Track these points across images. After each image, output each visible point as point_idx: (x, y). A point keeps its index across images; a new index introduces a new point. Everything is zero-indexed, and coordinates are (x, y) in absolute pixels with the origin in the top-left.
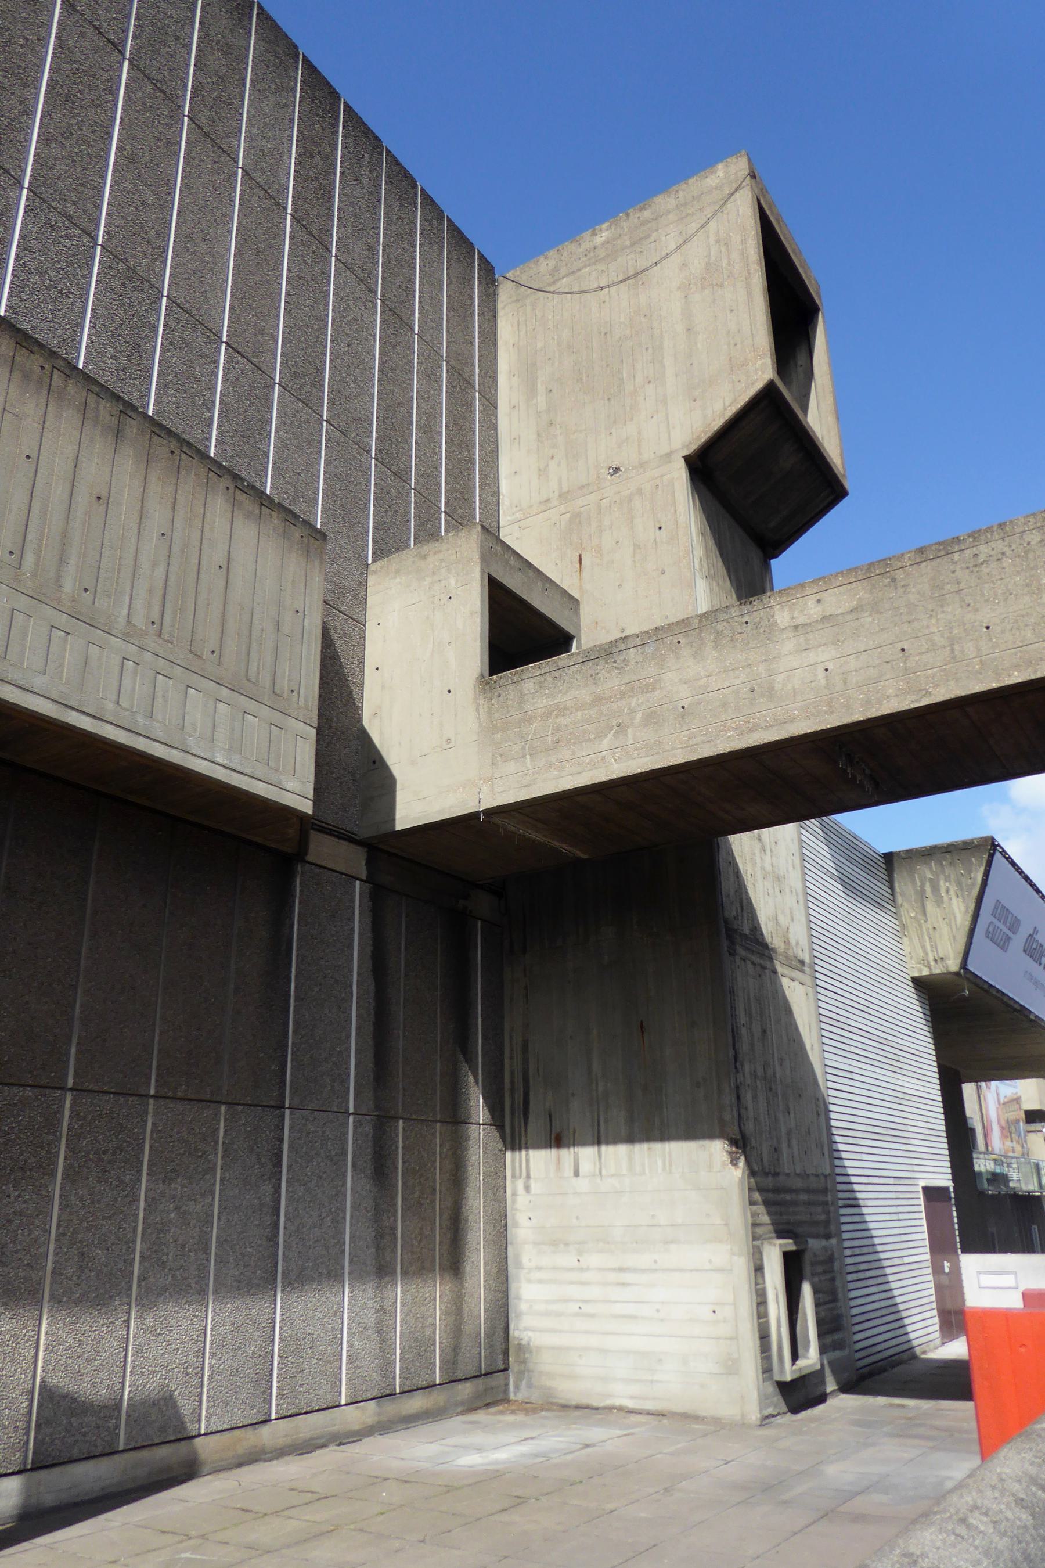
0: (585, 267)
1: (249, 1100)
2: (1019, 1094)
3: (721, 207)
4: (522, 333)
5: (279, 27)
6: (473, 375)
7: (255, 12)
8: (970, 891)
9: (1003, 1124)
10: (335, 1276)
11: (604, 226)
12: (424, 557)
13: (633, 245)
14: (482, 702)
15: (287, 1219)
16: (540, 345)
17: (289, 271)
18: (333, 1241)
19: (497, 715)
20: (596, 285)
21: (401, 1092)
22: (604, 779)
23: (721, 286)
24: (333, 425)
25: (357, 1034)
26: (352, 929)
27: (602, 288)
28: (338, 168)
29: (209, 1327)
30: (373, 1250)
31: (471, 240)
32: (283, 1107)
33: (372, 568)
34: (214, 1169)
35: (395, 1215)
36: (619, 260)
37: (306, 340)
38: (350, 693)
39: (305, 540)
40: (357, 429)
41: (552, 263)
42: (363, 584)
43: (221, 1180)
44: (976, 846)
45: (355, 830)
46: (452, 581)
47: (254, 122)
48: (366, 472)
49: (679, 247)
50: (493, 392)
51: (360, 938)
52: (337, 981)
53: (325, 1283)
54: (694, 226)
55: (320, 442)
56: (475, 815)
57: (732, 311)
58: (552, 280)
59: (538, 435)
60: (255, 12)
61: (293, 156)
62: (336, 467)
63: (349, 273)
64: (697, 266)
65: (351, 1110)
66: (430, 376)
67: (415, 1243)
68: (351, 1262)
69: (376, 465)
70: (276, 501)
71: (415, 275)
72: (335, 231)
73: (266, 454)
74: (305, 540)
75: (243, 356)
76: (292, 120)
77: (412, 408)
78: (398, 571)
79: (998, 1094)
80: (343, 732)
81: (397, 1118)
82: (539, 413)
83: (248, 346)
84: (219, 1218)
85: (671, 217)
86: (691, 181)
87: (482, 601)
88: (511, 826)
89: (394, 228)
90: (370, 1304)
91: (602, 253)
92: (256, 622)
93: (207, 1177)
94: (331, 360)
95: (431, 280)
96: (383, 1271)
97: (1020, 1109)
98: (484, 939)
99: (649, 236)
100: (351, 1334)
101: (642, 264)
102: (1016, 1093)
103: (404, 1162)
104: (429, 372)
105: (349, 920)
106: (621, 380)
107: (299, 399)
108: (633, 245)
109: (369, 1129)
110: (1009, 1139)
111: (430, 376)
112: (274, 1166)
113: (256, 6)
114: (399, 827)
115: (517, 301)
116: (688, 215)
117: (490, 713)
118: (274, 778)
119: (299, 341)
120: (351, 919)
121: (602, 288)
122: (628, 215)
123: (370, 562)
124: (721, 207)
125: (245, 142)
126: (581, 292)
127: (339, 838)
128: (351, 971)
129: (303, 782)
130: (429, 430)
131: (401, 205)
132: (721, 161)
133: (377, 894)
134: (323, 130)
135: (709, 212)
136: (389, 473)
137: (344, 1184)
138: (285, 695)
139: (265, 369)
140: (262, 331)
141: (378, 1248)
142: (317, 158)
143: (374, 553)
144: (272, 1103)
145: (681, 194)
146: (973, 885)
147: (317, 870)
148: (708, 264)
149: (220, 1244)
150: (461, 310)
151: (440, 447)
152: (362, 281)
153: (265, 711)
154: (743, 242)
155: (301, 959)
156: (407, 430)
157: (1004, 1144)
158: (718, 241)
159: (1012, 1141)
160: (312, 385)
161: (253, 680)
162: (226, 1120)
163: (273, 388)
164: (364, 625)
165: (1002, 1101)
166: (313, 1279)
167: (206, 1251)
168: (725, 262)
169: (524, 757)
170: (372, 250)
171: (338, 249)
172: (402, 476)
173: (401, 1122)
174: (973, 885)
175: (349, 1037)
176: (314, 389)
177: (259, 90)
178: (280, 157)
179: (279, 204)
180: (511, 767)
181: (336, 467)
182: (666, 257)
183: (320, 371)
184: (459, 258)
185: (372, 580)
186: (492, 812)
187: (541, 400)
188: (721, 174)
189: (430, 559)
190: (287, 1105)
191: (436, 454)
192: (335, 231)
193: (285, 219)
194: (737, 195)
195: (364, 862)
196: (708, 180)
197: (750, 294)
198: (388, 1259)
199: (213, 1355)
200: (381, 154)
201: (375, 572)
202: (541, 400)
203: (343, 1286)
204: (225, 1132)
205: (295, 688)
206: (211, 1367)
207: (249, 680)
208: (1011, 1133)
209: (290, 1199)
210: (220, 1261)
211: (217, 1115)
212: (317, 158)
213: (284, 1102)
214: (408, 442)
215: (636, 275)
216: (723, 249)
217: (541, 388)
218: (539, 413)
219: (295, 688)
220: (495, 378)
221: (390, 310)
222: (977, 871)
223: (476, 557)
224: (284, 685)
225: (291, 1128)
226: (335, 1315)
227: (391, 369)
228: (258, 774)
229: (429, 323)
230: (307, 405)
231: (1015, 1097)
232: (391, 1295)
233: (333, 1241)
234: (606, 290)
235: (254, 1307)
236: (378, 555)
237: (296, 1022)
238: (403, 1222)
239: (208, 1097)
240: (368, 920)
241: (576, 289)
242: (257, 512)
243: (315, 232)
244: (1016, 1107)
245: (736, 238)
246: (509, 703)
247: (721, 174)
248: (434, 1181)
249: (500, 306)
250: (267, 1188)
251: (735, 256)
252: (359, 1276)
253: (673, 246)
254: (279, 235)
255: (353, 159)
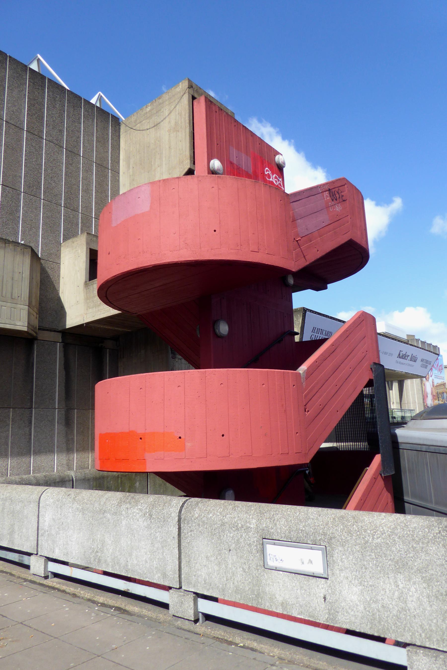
0: (144, 120)
1: (20, 407)
2: (445, 382)
3: (180, 100)
4: (127, 145)
5: (19, 62)
6: (108, 164)
7: (8, 60)
8: (298, 326)
9: (434, 394)
10: (52, 451)
11: (149, 104)
12: (73, 242)
13: (157, 112)
14: (85, 290)
15: (34, 437)
16: (131, 149)
17: (26, 151)
18: (50, 442)
19: (88, 294)
20: (146, 128)
21: (76, 402)
22: (110, 315)
23: (178, 131)
24: (45, 200)
25: (58, 387)
26: (56, 357)
27: (148, 129)
28: (46, 105)
29: (9, 463)
30: (65, 444)
31: (108, 111)
32: (32, 408)
33: (62, 245)
34: (9, 425)
35: (74, 435)
36: (153, 118)
37: (33, 174)
38: (54, 286)
39: (23, 250)
40: (55, 198)
41: (135, 117)
42: (59, 251)
43: (12, 428)
44: (299, 311)
45: (57, 328)
46: (80, 251)
47: (9, 102)
48: (60, 212)
49: (169, 115)
50: (118, 167)
51: (59, 359)
52: (50, 372)
53: (48, 453)
54: (173, 107)
55: (40, 207)
56: (83, 325)
57: (181, 141)
58: (135, 125)
59: (130, 184)
60: (8, 60)
61: (26, 108)
62: (47, 214)
63: (51, 143)
64: (173, 122)
65: (57, 408)
66: (88, 170)
67: (81, 442)
68: (57, 447)
69: (64, 209)
70: (11, 240)
71: (81, 134)
72: (45, 130)
73: (19, 217)
74: (23, 250)
75: (8, 187)
76: (25, 95)
77: (80, 184)
78: (68, 247)
79: (433, 382)
80: (52, 299)
81: (75, 409)
82: (130, 175)
83: (10, 183)
84: (11, 437)
85: (167, 103)
86: (173, 89)
87: (86, 258)
88: (97, 326)
89: (71, 119)
90: (64, 458)
91: (148, 115)
92: (4, 279)
93: (7, 427)
94: (44, 177)
95: (88, 134)
96: (69, 450)
97: (445, 388)
98: (110, 355)
99: (160, 110)
100: (57, 466)
101: (159, 120)
102: (444, 382)
103: (77, 421)
104: (87, 169)
105: (55, 355)
106: (152, 165)
107: (31, 195)
108: (157, 112)
109: (63, 412)
110: (437, 400)
111: (88, 170)
112: (29, 423)
113: (8, 57)
114: (67, 327)
115: (126, 132)
116: (171, 102)
117: (86, 294)
118: (13, 323)
119: (31, 175)
120: (56, 354)
121: (148, 129)
122: (155, 100)
123: (62, 243)
124: (180, 100)
125: (6, 111)
126: (143, 130)
127: (51, 331)
128: (56, 369)
129: (23, 322)
130: (87, 191)
131: (74, 109)
132: (181, 82)
133: (66, 346)
134: (39, 93)
135: (177, 101)
136: (69, 210)
137: (55, 427)
138: (16, 299)
139: (17, 189)
140: (16, 176)
141: (67, 444)
142: (36, 105)
143: (63, 239)
144: (28, 407)
145: (170, 94)
146: (299, 324)
147: (42, 342)
148: (176, 122)
149: (12, 443)
150: (102, 141)
151: (92, 195)
152: (57, 145)
153: (9, 304)
154: (185, 115)
155: (37, 367)
156: (78, 193)
157: (433, 402)
158: (178, 114)
159: (439, 401)
160: (36, 189)
161: (4, 296)
162: (12, 412)
163: (21, 194)
164: (60, 264)
165: (435, 385)
166: (44, 452)
167: (7, 445)
168: (180, 123)
169: (93, 308)
170: (61, 131)
171: (46, 136)
172: (75, 210)
173: (76, 410)
174: (299, 324)
175: (55, 388)
176: (37, 190)
177: (11, 89)
178: (20, 111)
179: (21, 128)
180: (90, 310)
181: (47, 214)
182: (165, 119)
183: (40, 183)
184: (102, 121)
185: (62, 248)
186: (87, 324)
187: (131, 170)
188: (180, 87)
189: (75, 243)
190: (33, 407)
191: (90, 198)
192: (45, 130)
193: (24, 133)
194: (184, 96)
195: (60, 337)
196: (177, 89)
197: (185, 135)
198: (71, 447)
199: (10, 470)
200: (65, 93)
201: (63, 246)
202: (131, 170)
203: (55, 454)
204: (12, 415)
205: (20, 295)
206: (10, 473)
207: (2, 296)
208: (438, 398)
209: (35, 432)
210: (12, 447)
211: (9, 411)
212: (36, 105)
213: (32, 407)
214: (78, 197)
215: (157, 124)
216: (180, 117)
217: (131, 166)
218: (130, 175)
219: (20, 295)
220: (118, 162)
221: (70, 151)
222: (300, 319)
223: (85, 243)
224: (15, 295)
225: (35, 413)
226: (52, 461)
227: (70, 173)
228: (7, 322)
229: (88, 150)
230: (34, 196)
231: (443, 383)
232: (72, 456)
233: (50, 442)
234: (149, 130)
235: (24, 459)
236: (64, 240)
237: (36, 385)
238: (76, 437)
239: (6, 407)
240: (62, 354)
241: (141, 129)
242: (4, 246)
243: (36, 133)
244: (443, 387)
245: (183, 113)
246: (91, 291)
247: (180, 87)
248: (89, 425)
249: (121, 133)
250: (27, 429)
251: (183, 120)
252: (60, 451)
253: (167, 114)
254: (21, 140)
255: (52, 100)
